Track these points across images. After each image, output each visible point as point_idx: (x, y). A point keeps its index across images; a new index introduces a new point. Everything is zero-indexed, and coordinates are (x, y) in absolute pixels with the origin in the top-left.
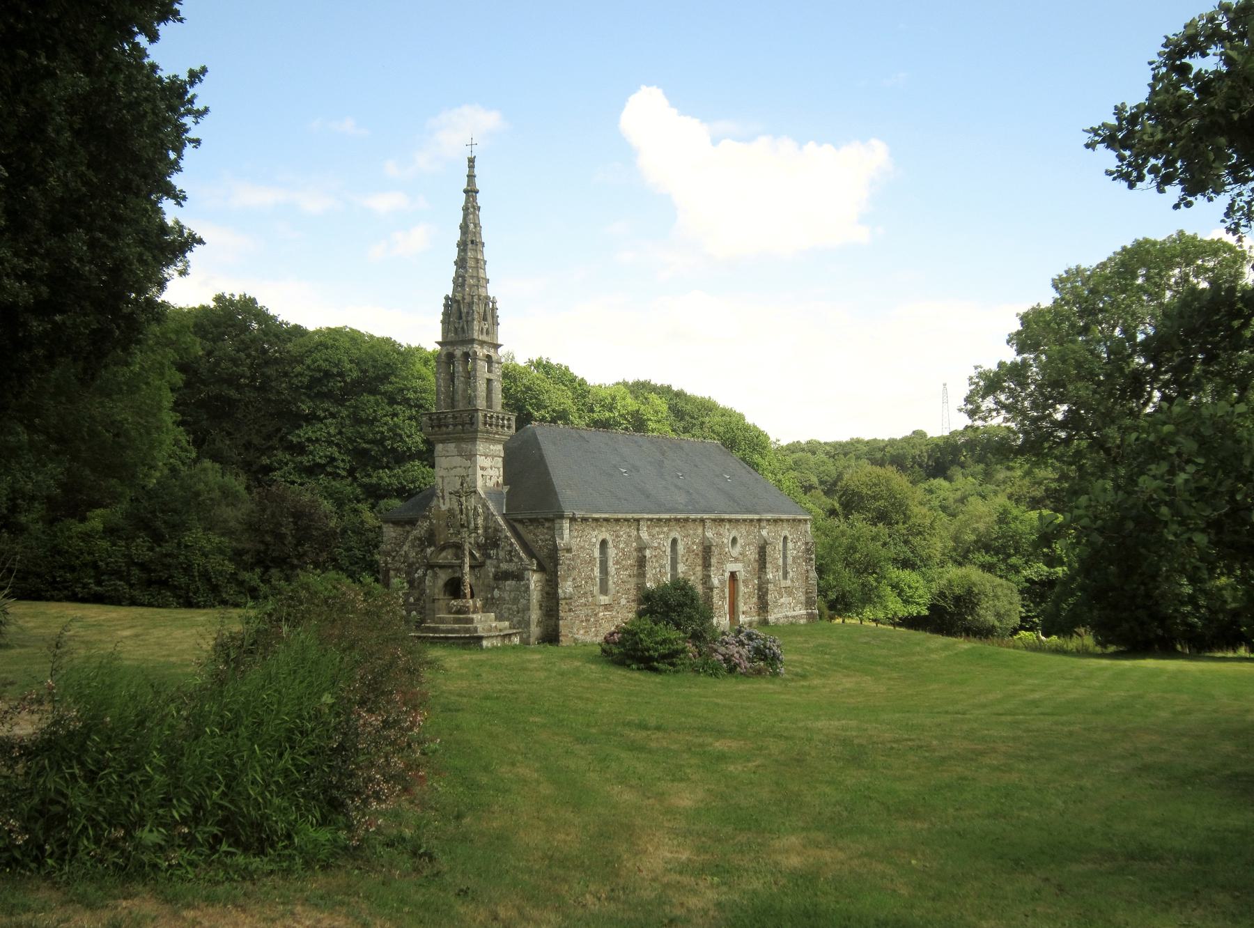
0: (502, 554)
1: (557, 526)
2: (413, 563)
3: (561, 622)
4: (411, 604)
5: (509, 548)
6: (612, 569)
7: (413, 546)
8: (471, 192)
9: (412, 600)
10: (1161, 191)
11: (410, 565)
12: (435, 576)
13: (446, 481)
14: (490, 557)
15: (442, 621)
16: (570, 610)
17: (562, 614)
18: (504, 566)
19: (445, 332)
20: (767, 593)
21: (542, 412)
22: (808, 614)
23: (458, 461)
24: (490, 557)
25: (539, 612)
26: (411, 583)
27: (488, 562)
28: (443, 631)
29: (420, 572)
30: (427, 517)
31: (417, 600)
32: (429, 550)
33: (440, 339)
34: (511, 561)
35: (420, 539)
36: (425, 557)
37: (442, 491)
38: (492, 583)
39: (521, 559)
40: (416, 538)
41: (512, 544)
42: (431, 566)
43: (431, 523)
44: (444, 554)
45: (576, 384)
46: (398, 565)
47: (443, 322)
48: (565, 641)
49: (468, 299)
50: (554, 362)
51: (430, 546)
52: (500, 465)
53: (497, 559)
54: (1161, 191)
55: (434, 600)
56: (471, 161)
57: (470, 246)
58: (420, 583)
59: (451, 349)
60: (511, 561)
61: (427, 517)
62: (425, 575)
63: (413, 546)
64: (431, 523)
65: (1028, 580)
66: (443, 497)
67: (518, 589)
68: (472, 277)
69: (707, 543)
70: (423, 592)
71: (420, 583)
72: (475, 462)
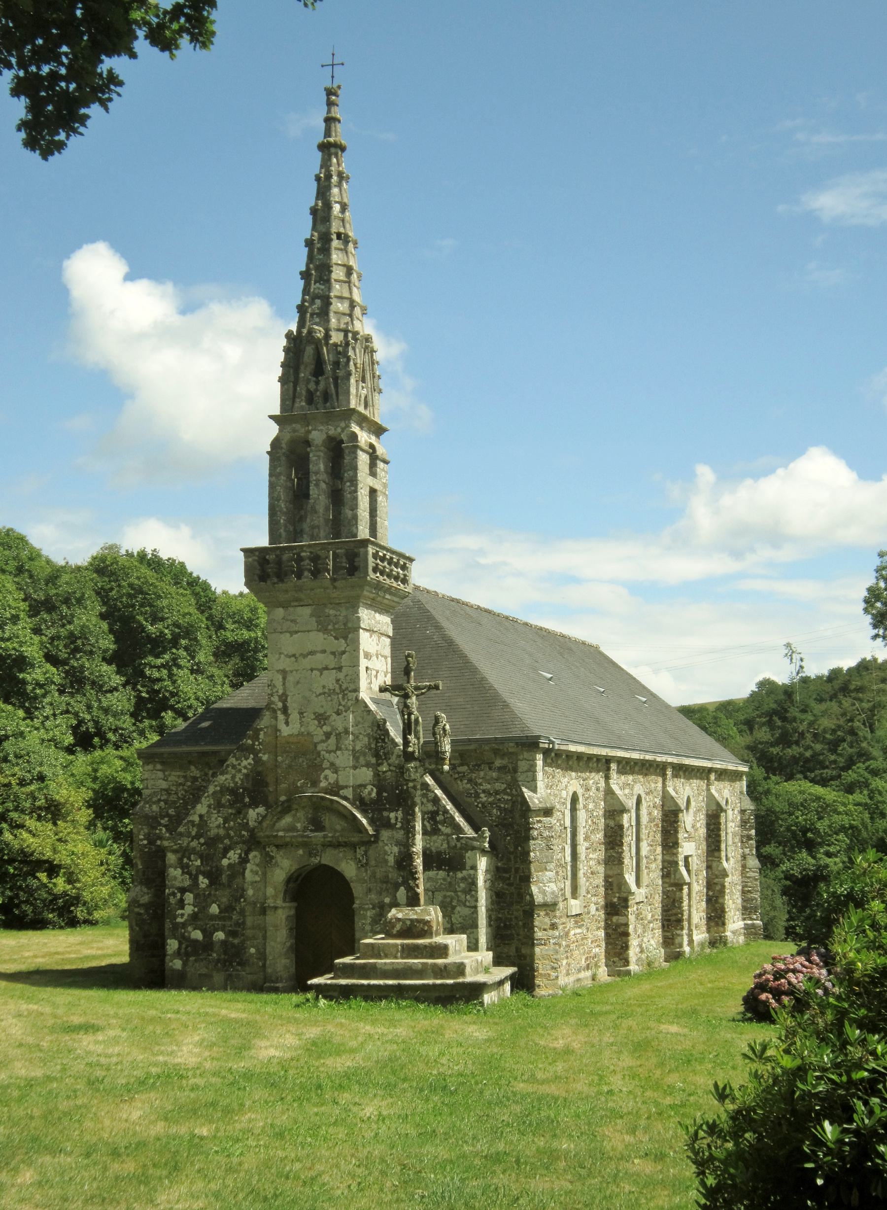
1: (522, 765)
2: (218, 839)
3: (537, 950)
4: (213, 917)
6: (582, 849)
7: (219, 805)
9: (214, 909)
11: (212, 842)
12: (268, 861)
13: (290, 679)
14: (388, 825)
15: (375, 951)
16: (554, 926)
17: (539, 934)
19: (288, 398)
20: (722, 892)
21: (160, 626)
22: (747, 927)
23: (317, 640)
24: (388, 825)
26: (214, 877)
27: (385, 834)
28: (385, 975)
29: (233, 856)
30: (250, 750)
31: (227, 910)
32: (253, 814)
33: (277, 412)
35: (233, 792)
36: (245, 826)
39: (458, 829)
40: (224, 790)
41: (436, 800)
42: (253, 842)
43: (257, 760)
44: (287, 820)
45: (198, 589)
47: (283, 380)
48: (543, 990)
49: (336, 338)
50: (164, 555)
51: (254, 804)
52: (387, 651)
55: (264, 911)
57: (335, 243)
58: (232, 877)
59: (301, 430)
61: (250, 750)
62: (244, 861)
63: (219, 805)
64: (257, 760)
65: (788, 876)
66: (285, 710)
67: (451, 886)
68: (341, 298)
69: (670, 807)
70: (240, 894)
71: (232, 877)
72: (356, 642)
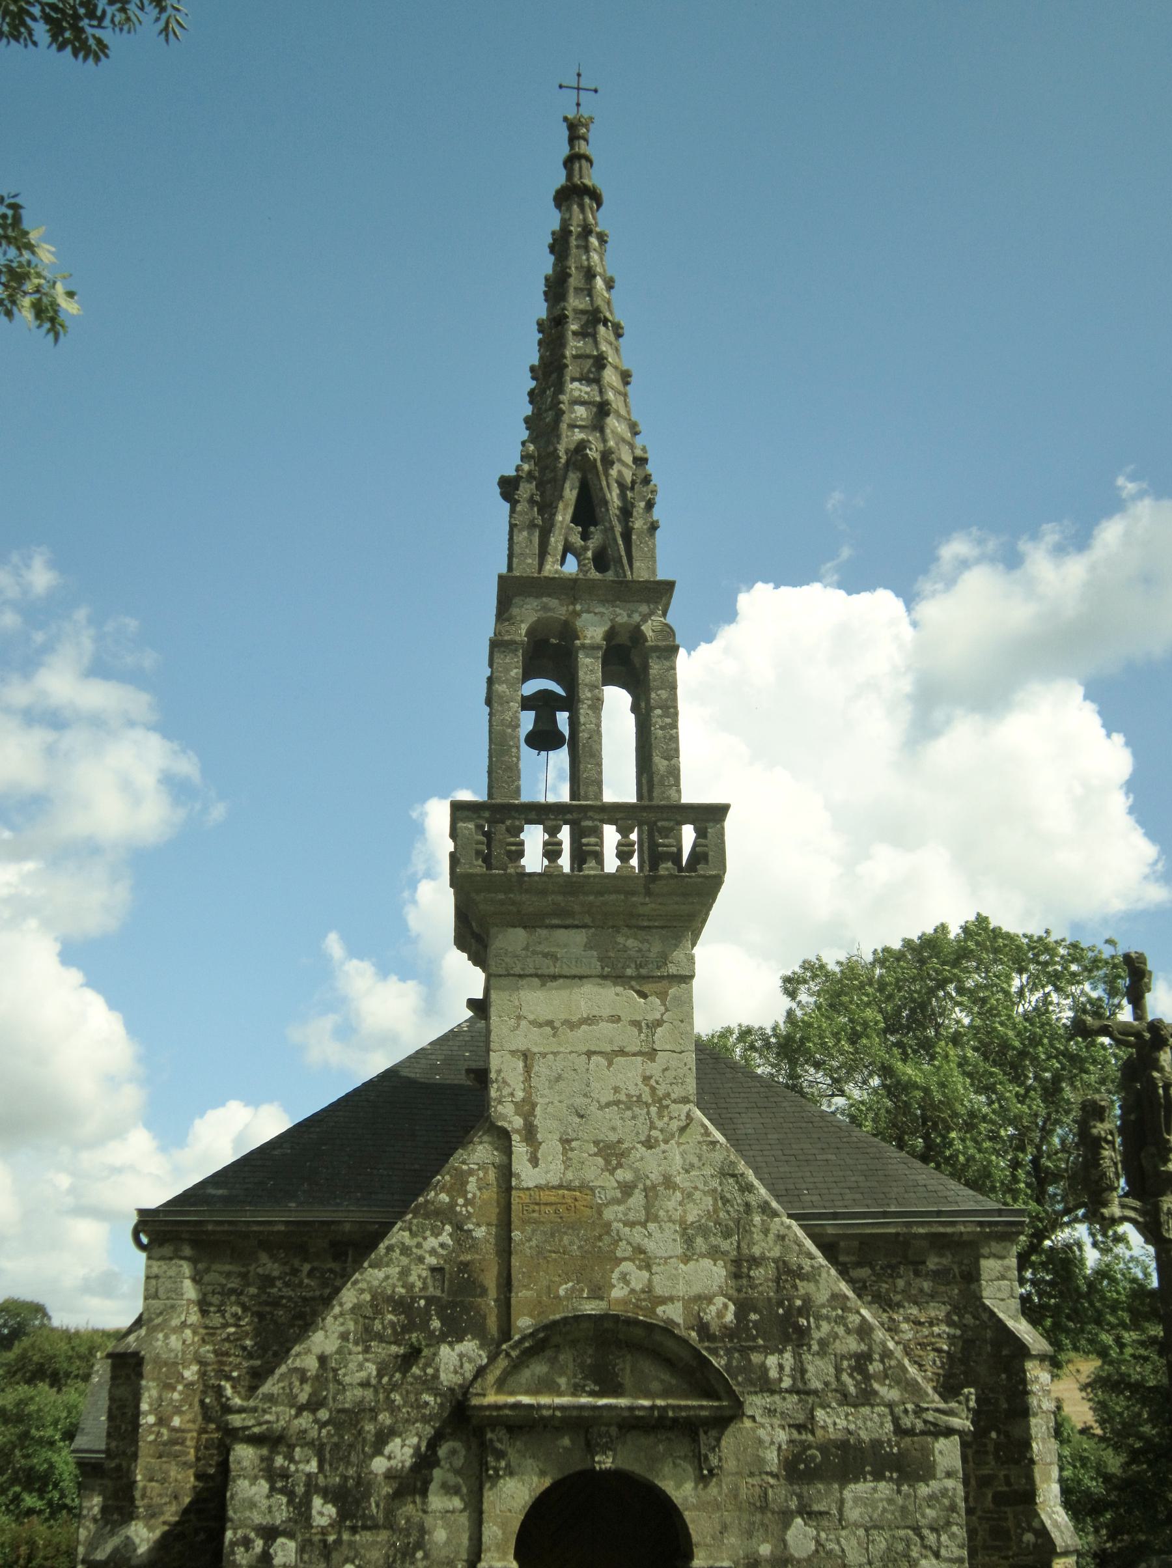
0: (819, 1371)
5: (852, 1344)
7: (367, 1336)
8: (574, 194)
10: (591, 119)
13: (540, 1068)
18: (833, 1421)
25: (580, 1396)
34: (867, 1397)
35: (402, 1305)
37: (527, 1108)
38: (781, 1494)
40: (380, 1301)
46: (280, 1417)
51: (454, 1332)
53: (801, 1390)
54: (591, 119)
56: (575, 130)
60: (867, 1397)
63: (367, 1336)
